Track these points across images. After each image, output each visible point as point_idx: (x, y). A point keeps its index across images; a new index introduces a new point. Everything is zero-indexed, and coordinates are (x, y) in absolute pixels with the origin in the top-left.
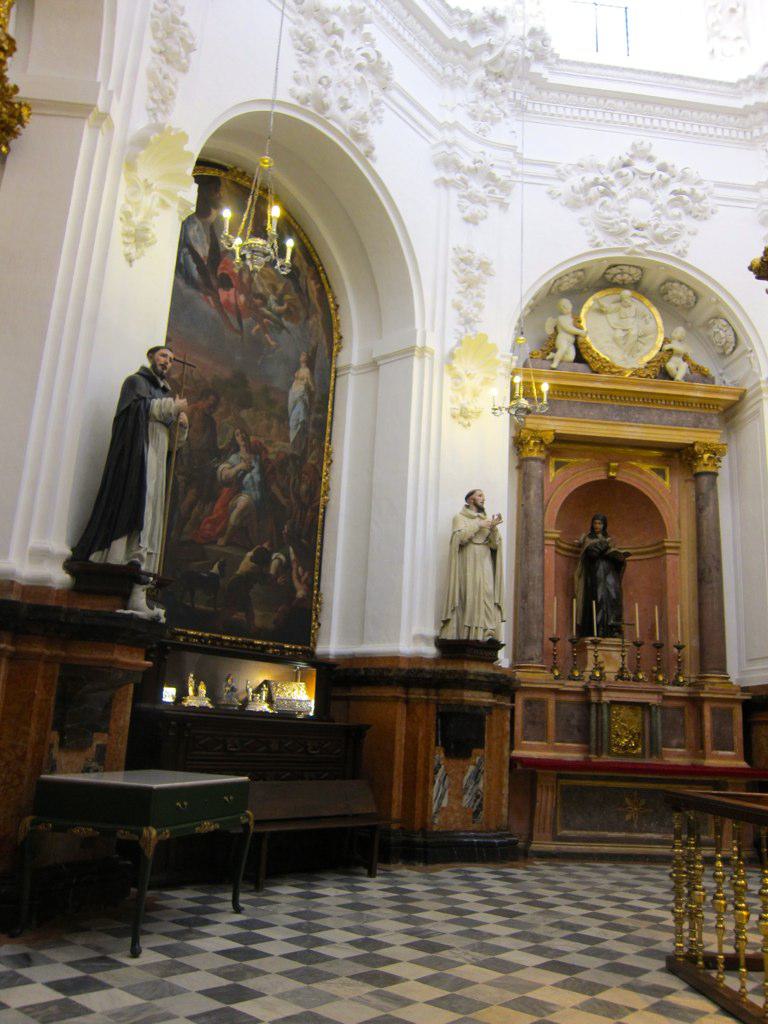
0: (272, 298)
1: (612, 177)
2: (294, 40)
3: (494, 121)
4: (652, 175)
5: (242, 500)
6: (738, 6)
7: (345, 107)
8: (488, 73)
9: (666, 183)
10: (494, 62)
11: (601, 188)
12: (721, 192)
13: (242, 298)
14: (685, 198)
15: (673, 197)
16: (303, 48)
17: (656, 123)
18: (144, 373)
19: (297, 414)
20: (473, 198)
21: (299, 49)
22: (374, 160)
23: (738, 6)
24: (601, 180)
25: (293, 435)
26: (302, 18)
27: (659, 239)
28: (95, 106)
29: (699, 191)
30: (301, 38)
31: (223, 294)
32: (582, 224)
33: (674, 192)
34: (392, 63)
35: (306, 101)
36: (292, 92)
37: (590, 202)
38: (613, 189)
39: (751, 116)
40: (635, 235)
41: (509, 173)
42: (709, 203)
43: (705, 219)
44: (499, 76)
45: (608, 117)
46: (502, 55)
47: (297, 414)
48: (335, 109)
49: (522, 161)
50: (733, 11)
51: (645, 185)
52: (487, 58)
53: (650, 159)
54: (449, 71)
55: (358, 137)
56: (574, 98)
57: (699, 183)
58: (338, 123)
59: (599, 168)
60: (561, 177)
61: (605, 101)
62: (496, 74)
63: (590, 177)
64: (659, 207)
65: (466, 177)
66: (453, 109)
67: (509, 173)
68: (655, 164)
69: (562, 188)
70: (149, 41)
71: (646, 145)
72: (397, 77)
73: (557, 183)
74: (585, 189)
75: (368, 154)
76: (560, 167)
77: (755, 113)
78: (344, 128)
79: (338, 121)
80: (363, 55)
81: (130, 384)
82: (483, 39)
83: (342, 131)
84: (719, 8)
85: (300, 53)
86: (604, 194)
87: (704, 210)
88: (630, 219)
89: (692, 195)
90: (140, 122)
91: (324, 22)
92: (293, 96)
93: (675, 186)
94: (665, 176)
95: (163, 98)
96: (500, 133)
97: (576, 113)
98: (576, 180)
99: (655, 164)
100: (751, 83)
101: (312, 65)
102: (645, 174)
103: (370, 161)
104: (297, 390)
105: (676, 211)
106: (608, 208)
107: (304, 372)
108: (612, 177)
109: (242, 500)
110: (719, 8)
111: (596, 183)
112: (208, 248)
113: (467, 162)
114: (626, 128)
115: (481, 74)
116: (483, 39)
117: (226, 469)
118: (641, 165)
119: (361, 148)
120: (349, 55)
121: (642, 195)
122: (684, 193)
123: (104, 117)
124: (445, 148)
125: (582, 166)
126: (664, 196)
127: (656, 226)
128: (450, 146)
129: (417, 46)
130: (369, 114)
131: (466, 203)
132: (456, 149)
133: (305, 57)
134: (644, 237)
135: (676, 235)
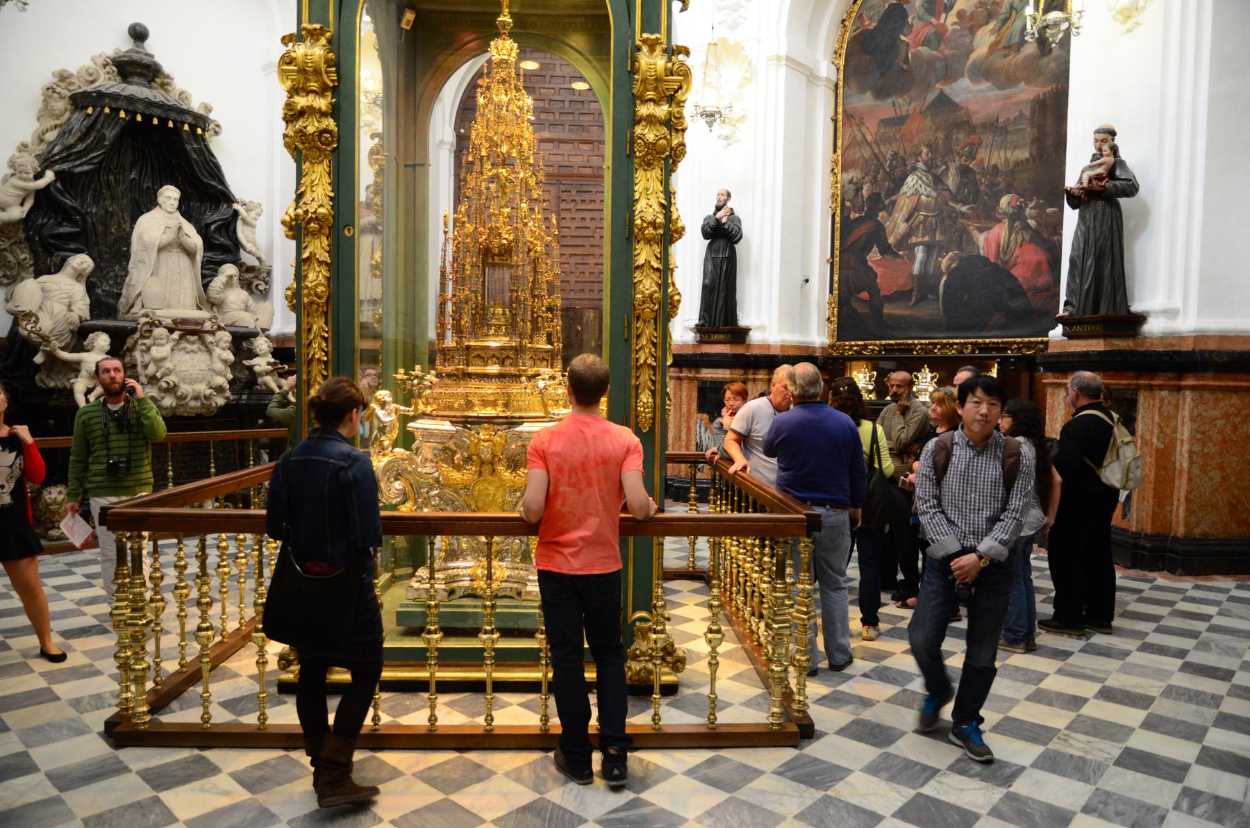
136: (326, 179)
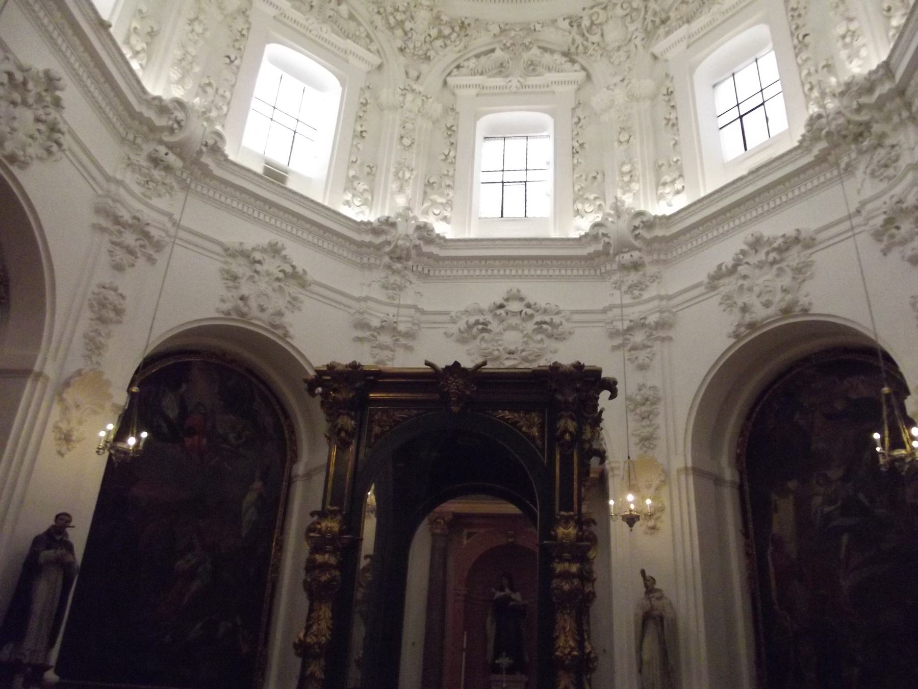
0: (232, 436)
1: (489, 317)
2: (223, 275)
3: (401, 288)
4: (521, 312)
5: (195, 586)
6: (598, 173)
7: (262, 309)
8: (391, 258)
9: (532, 316)
10: (393, 251)
11: (480, 327)
12: (576, 317)
13: (204, 441)
14: (545, 326)
15: (536, 326)
16: (229, 278)
17: (526, 272)
18: (53, 527)
19: (249, 515)
20: (382, 347)
21: (227, 279)
22: (291, 338)
23: (598, 173)
24: (481, 320)
25: (244, 533)
26: (229, 260)
27: (525, 359)
28: (32, 370)
29: (557, 319)
30: (228, 272)
31: (188, 441)
32: (468, 354)
33: (537, 323)
34: (307, 269)
35: (229, 313)
36: (218, 310)
37: (475, 338)
38: (489, 327)
39: (596, 260)
40: (507, 359)
41: (410, 325)
42: (567, 326)
43: (564, 339)
44: (399, 259)
45: (489, 272)
46: (396, 246)
47: (249, 515)
48: (255, 312)
49: (423, 312)
50: (595, 178)
51: (515, 321)
52: (388, 249)
53: (522, 299)
54: (365, 260)
55: (275, 327)
56: (463, 262)
57: (558, 313)
58: (259, 323)
59: (481, 312)
60: (454, 322)
61: (486, 262)
62: (397, 258)
63: (472, 320)
64: (526, 336)
65: (375, 334)
66: (370, 285)
67: (410, 325)
68: (524, 303)
69: (453, 329)
70: (87, 314)
71: (515, 291)
72: (312, 275)
73: (450, 326)
74: (470, 327)
75: (286, 335)
76: (453, 314)
77: (599, 256)
78: (263, 322)
79: (259, 319)
80: (280, 271)
81: (37, 541)
82: (382, 238)
83: (263, 325)
84: (584, 177)
85: (227, 282)
86: (484, 330)
87: (563, 333)
88: (501, 348)
89: (551, 323)
90: (76, 363)
91: (248, 257)
92: (218, 312)
93: (538, 318)
94: (529, 311)
95: (94, 346)
96: (407, 297)
97: (466, 273)
98: (462, 324)
99: (524, 303)
100: (589, 238)
101: (236, 288)
102: (515, 312)
103: (288, 339)
104: (251, 497)
105: (539, 337)
106: (486, 341)
107: (258, 484)
108: (489, 317)
109: (195, 586)
110: (584, 177)
111: (477, 323)
112: (177, 411)
113: (375, 323)
114: (497, 279)
115: (386, 259)
116: (382, 238)
117: (181, 565)
118: (514, 306)
119: (280, 332)
120: (268, 274)
121: (515, 328)
122: (545, 323)
123: (39, 375)
124: (358, 316)
125: (468, 312)
126: (530, 326)
127: (523, 350)
128: (362, 313)
129: (336, 250)
130: (382, 266)
131: (377, 351)
132: (366, 315)
133: (231, 284)
134: (515, 359)
135: (539, 356)
136: (329, 614)
